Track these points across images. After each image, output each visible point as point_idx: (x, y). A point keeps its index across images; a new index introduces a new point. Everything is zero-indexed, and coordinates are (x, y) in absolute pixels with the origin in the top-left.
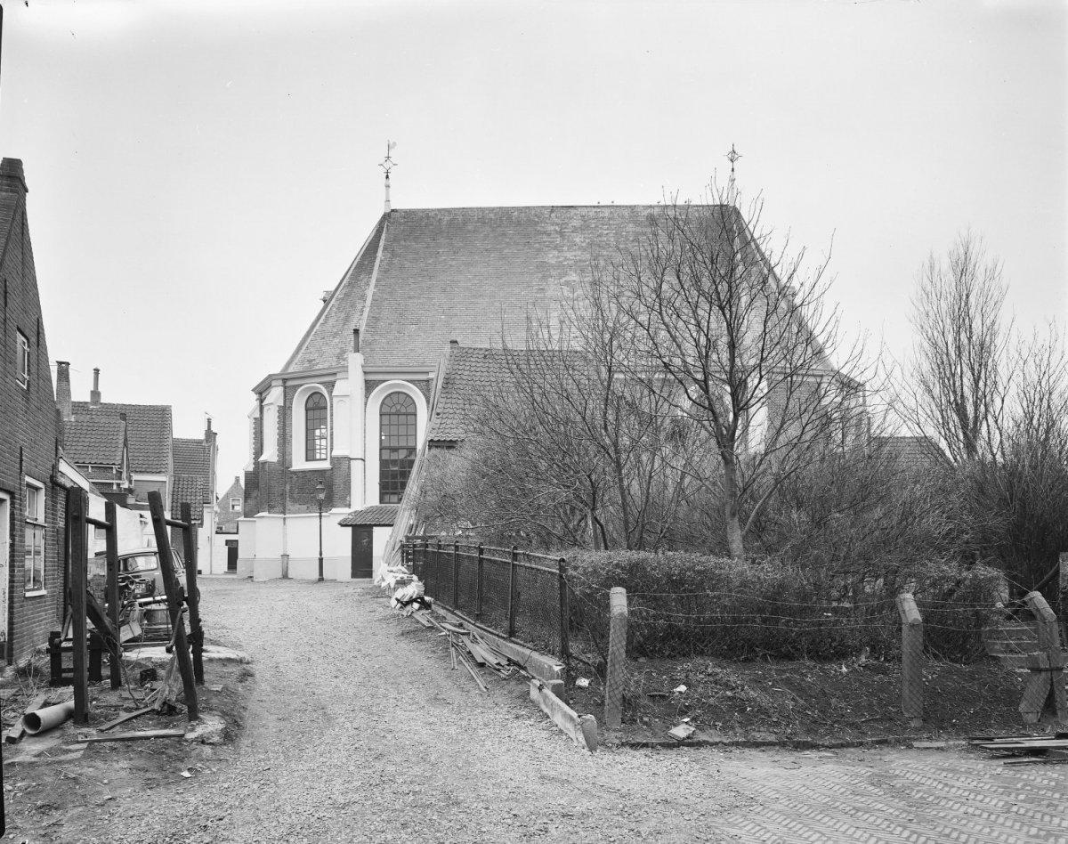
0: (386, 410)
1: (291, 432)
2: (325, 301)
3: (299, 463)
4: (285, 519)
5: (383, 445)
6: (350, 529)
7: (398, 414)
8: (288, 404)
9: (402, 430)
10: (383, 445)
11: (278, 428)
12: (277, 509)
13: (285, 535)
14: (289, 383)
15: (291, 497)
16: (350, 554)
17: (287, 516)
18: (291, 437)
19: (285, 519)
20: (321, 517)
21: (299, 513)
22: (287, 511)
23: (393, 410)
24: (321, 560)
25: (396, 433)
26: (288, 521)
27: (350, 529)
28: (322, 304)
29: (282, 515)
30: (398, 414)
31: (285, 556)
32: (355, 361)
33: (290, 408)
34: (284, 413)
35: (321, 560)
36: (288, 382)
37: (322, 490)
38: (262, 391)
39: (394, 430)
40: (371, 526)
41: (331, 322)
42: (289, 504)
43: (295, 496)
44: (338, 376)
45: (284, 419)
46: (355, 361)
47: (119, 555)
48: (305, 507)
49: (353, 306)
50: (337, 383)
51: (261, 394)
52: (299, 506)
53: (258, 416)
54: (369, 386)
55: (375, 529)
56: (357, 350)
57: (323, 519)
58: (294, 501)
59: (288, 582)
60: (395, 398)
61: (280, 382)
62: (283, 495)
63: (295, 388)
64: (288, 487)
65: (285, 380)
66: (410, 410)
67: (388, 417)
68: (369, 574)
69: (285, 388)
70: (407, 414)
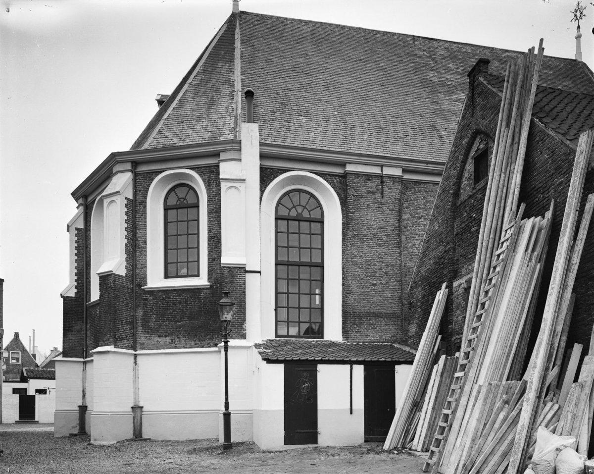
0: (284, 212)
1: (145, 235)
2: (160, 102)
3: (156, 278)
4: (135, 356)
5: (279, 259)
6: (281, 367)
7: (299, 219)
8: (140, 198)
9: (305, 241)
10: (279, 259)
11: (127, 229)
12: (124, 342)
13: (136, 378)
14: (142, 168)
15: (145, 327)
16: (282, 408)
17: (138, 352)
18: (145, 242)
19: (135, 356)
20: (226, 348)
21: (158, 348)
22: (138, 346)
23: (293, 213)
24: (227, 416)
25: (297, 244)
26: (139, 358)
27: (281, 367)
28: (156, 108)
29: (132, 352)
30: (299, 219)
31: (137, 409)
32: (251, 136)
33: (144, 203)
34: (135, 211)
35: (227, 416)
36: (140, 162)
37: (206, 316)
38: (88, 194)
39: (294, 240)
40: (315, 363)
41: (188, 107)
42: (142, 337)
43: (151, 324)
44: (223, 156)
45: (134, 218)
46: (251, 136)
47: (222, 262)
48: (168, 340)
49: (216, 90)
50: (221, 165)
51: (85, 197)
52: (157, 339)
53: (81, 225)
54: (266, 175)
55: (320, 367)
56: (250, 120)
57: (230, 352)
58: (150, 331)
59: (147, 447)
60: (295, 197)
61: (129, 166)
62: (133, 323)
63: (152, 175)
64: (140, 313)
65: (135, 164)
66: (315, 215)
67: (285, 222)
68: (312, 437)
69: (136, 175)
70: (310, 221)
